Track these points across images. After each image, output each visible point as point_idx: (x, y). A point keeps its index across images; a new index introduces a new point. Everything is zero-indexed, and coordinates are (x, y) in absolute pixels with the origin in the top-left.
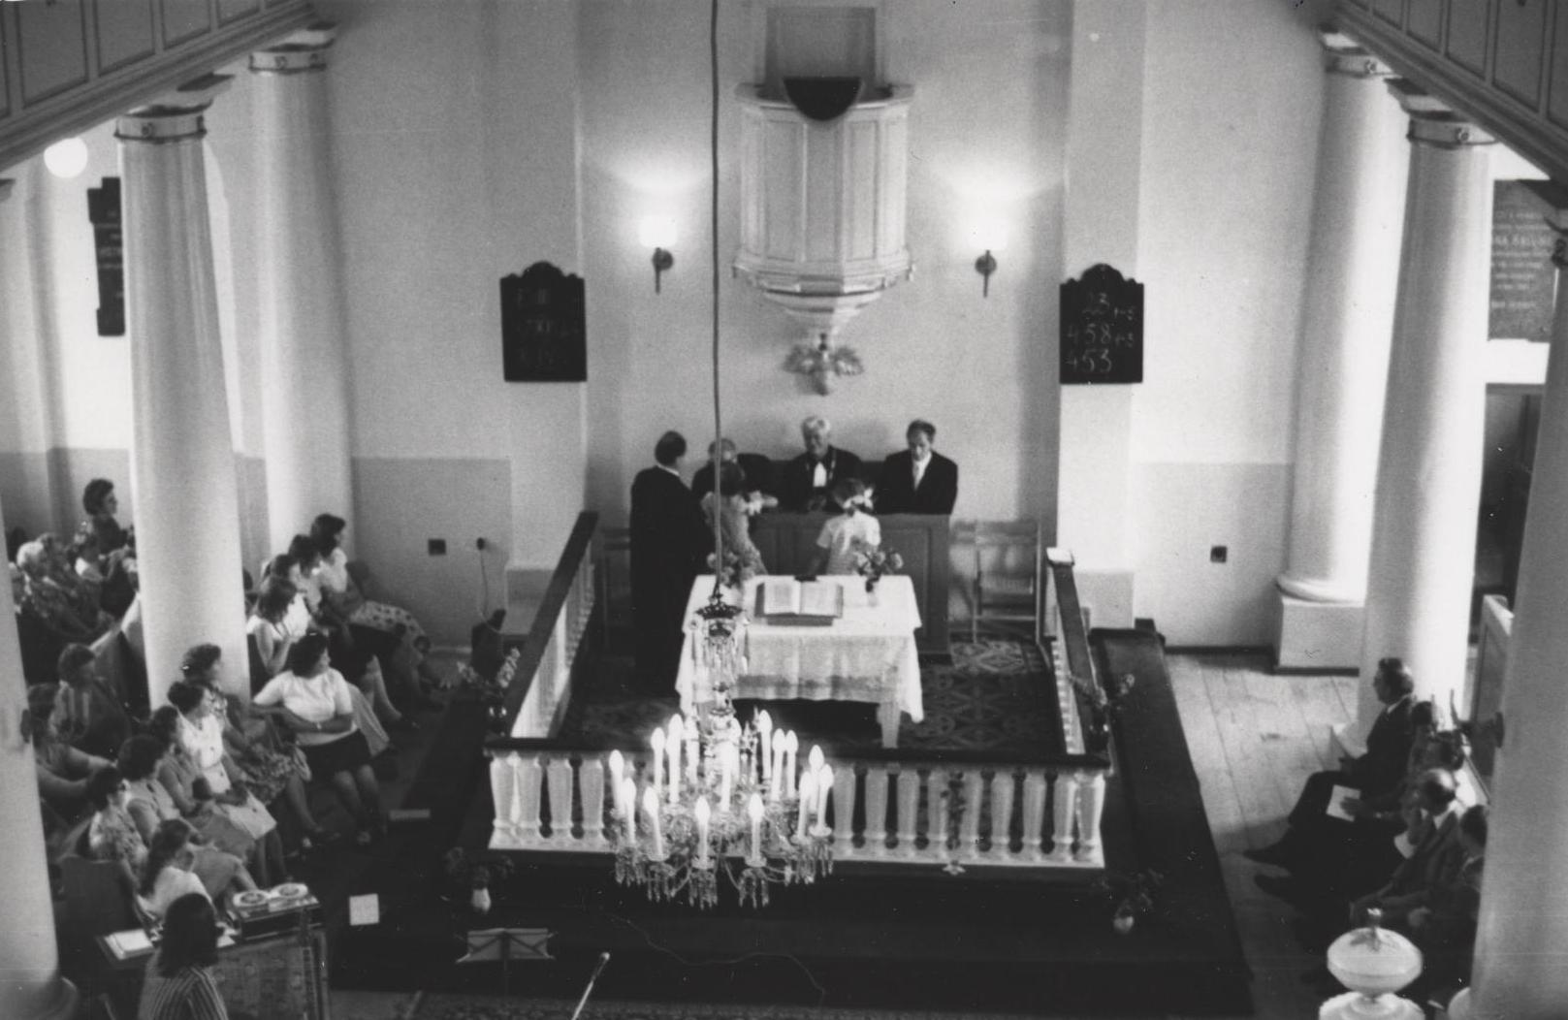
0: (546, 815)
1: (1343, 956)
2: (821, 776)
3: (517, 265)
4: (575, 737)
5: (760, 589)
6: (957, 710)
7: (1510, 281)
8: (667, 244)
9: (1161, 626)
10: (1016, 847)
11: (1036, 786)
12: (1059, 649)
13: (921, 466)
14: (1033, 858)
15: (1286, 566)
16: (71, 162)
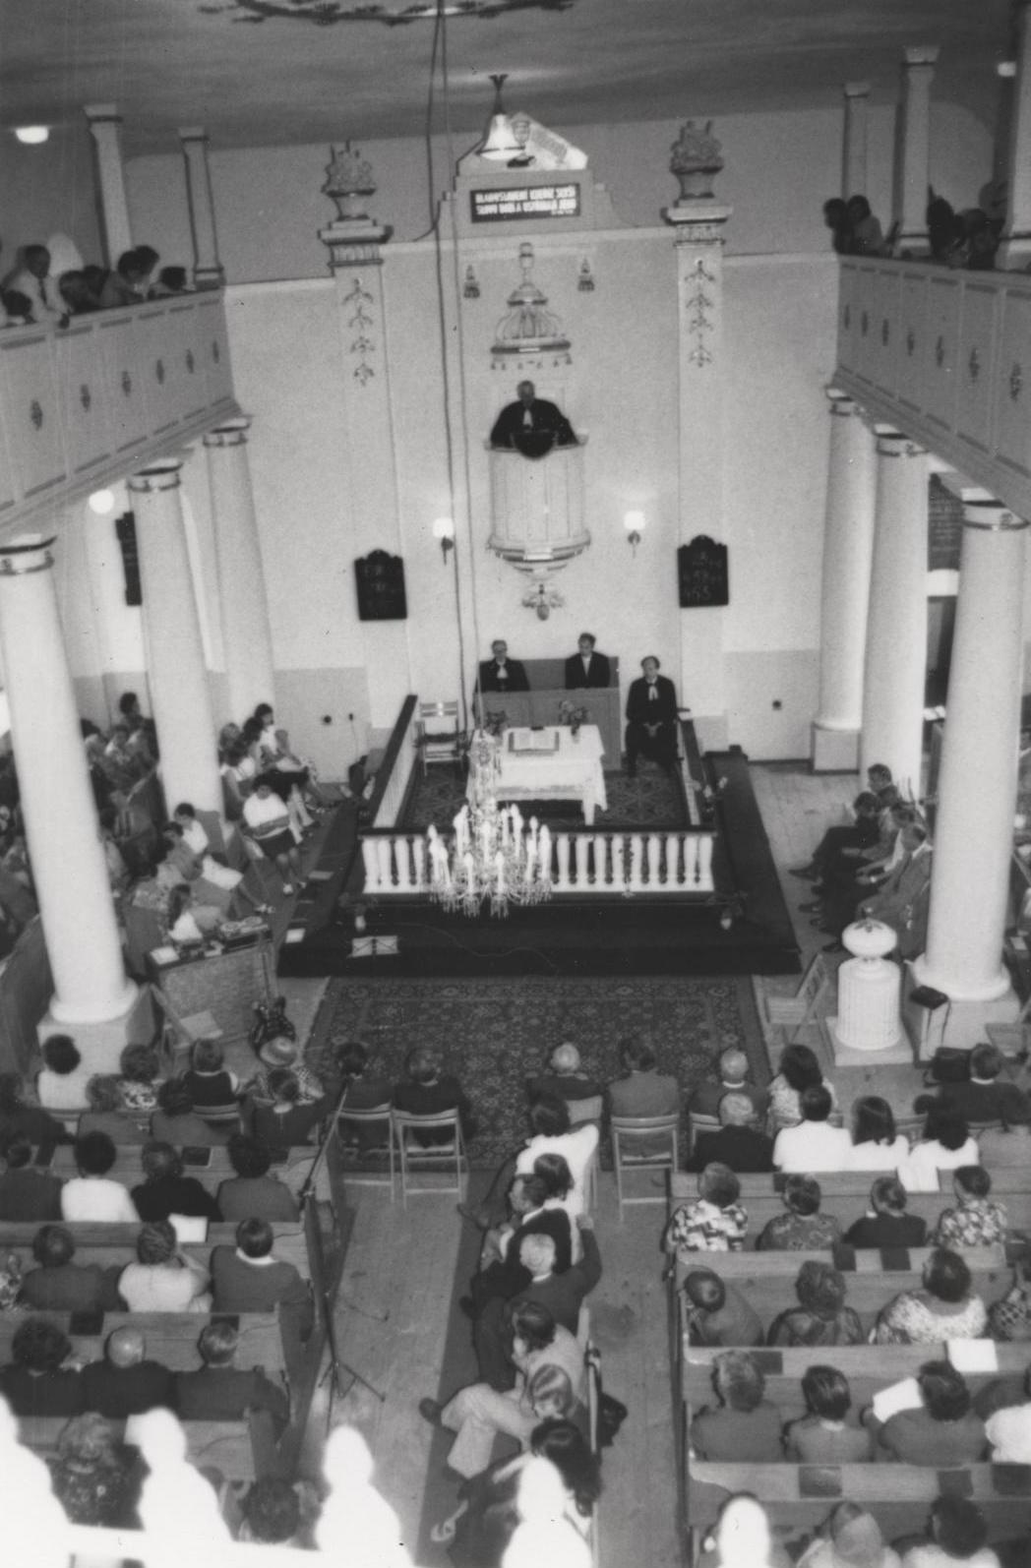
0: (394, 871)
1: (855, 938)
2: (541, 844)
3: (364, 551)
4: (408, 826)
5: (511, 736)
6: (627, 804)
7: (942, 534)
8: (449, 535)
9: (747, 749)
10: (663, 880)
11: (673, 844)
12: (685, 765)
13: (587, 661)
14: (672, 886)
15: (821, 708)
16: (106, 503)
